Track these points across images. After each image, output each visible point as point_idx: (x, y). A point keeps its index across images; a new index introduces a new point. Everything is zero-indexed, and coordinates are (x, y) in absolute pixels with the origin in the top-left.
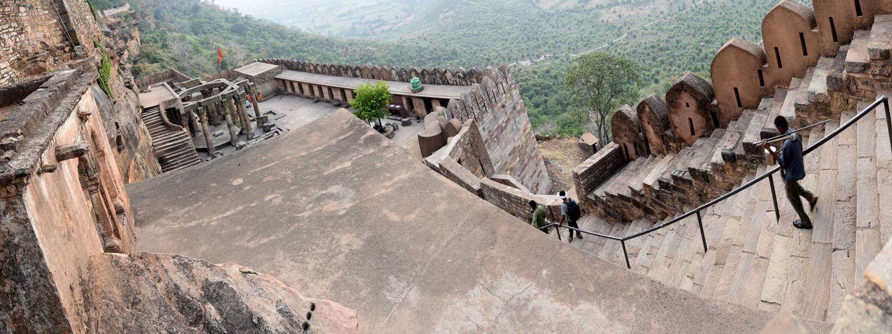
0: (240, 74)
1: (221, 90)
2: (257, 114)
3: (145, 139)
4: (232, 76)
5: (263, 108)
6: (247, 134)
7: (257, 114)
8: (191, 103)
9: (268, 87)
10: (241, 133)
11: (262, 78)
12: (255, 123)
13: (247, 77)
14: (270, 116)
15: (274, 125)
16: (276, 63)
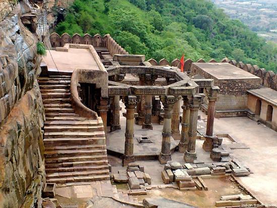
1: (169, 82)
5: (221, 126)
10: (176, 150)
11: (230, 86)
15: (227, 155)
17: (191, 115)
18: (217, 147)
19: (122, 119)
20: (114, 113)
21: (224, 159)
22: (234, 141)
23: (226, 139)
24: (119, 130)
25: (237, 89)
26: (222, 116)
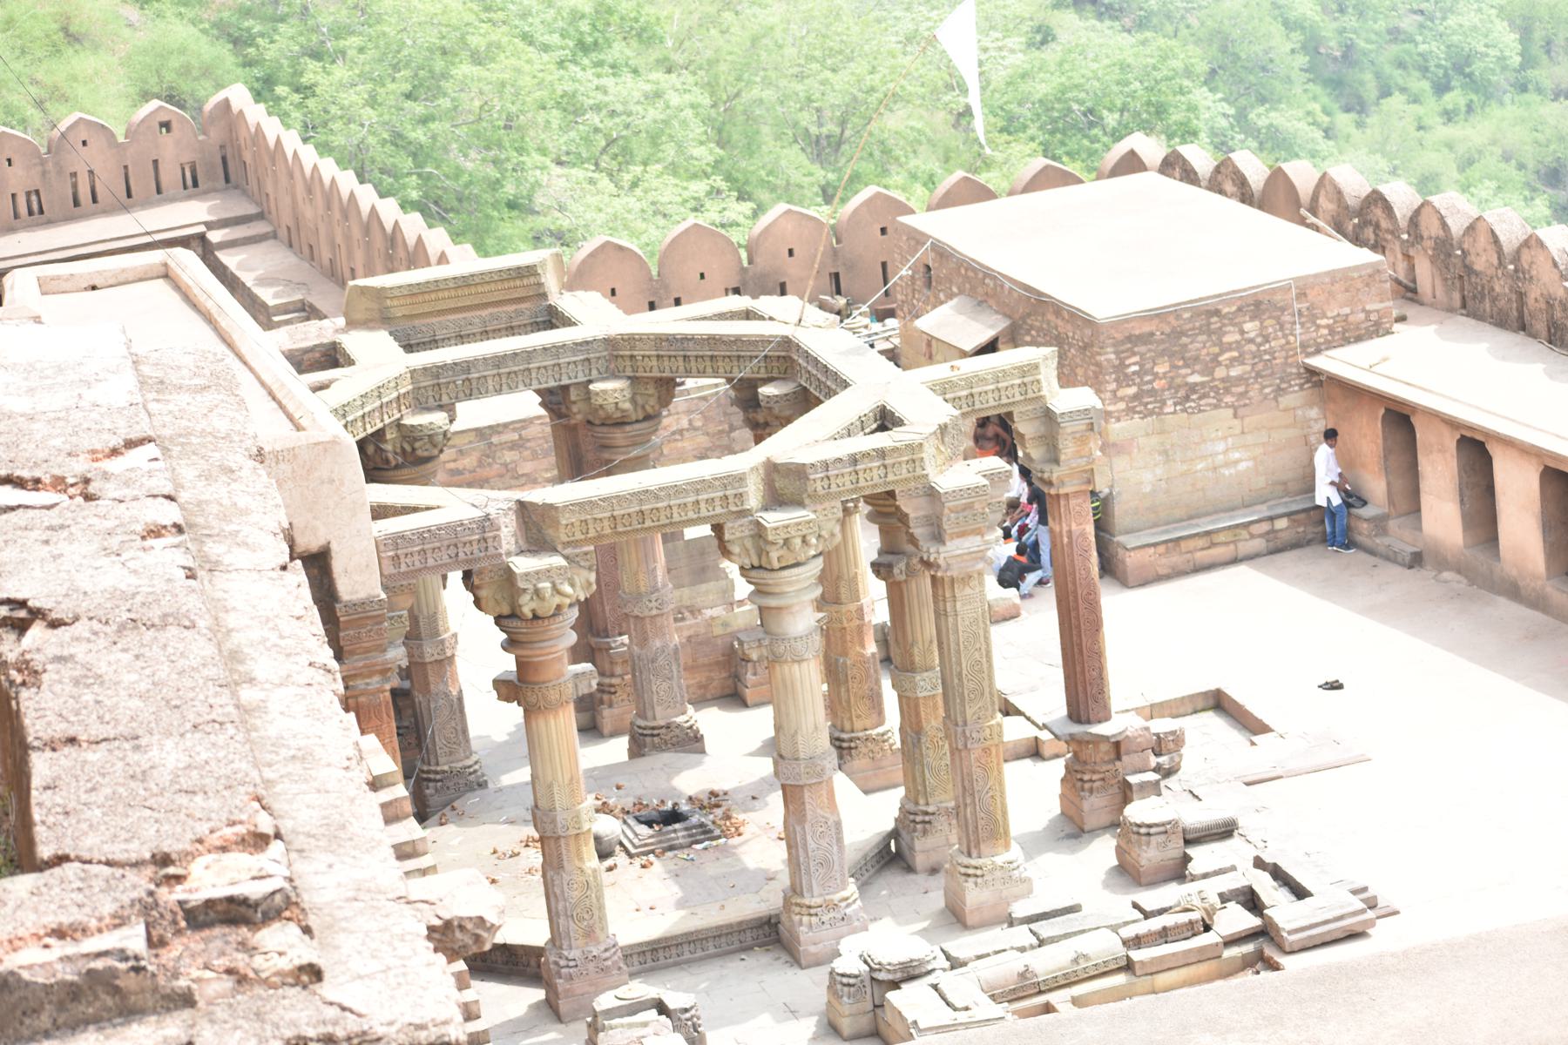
0: (946, 274)
1: (761, 420)
2: (1084, 688)
3: (98, 778)
4: (878, 276)
6: (956, 876)
7: (1084, 688)
8: (445, 505)
9: (1231, 450)
10: (891, 857)
11: (1170, 353)
12: (1055, 769)
13: (1027, 316)
14: (1206, 734)
15: (1225, 831)
16: (1363, 220)
17: (940, 615)
18: (1155, 789)
19: (491, 721)
20: (426, 690)
21: (1203, 857)
22: (1262, 728)
23: (1212, 722)
24: (471, 800)
25: (1239, 360)
26: (1164, 563)
